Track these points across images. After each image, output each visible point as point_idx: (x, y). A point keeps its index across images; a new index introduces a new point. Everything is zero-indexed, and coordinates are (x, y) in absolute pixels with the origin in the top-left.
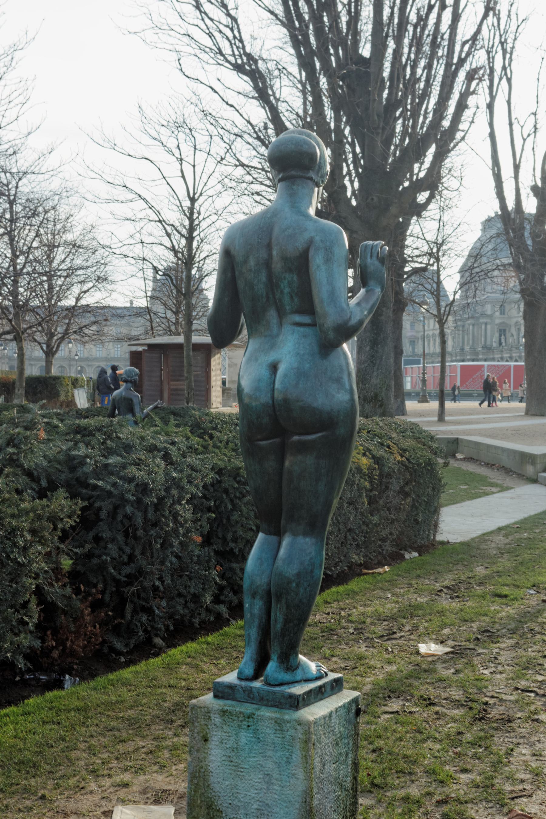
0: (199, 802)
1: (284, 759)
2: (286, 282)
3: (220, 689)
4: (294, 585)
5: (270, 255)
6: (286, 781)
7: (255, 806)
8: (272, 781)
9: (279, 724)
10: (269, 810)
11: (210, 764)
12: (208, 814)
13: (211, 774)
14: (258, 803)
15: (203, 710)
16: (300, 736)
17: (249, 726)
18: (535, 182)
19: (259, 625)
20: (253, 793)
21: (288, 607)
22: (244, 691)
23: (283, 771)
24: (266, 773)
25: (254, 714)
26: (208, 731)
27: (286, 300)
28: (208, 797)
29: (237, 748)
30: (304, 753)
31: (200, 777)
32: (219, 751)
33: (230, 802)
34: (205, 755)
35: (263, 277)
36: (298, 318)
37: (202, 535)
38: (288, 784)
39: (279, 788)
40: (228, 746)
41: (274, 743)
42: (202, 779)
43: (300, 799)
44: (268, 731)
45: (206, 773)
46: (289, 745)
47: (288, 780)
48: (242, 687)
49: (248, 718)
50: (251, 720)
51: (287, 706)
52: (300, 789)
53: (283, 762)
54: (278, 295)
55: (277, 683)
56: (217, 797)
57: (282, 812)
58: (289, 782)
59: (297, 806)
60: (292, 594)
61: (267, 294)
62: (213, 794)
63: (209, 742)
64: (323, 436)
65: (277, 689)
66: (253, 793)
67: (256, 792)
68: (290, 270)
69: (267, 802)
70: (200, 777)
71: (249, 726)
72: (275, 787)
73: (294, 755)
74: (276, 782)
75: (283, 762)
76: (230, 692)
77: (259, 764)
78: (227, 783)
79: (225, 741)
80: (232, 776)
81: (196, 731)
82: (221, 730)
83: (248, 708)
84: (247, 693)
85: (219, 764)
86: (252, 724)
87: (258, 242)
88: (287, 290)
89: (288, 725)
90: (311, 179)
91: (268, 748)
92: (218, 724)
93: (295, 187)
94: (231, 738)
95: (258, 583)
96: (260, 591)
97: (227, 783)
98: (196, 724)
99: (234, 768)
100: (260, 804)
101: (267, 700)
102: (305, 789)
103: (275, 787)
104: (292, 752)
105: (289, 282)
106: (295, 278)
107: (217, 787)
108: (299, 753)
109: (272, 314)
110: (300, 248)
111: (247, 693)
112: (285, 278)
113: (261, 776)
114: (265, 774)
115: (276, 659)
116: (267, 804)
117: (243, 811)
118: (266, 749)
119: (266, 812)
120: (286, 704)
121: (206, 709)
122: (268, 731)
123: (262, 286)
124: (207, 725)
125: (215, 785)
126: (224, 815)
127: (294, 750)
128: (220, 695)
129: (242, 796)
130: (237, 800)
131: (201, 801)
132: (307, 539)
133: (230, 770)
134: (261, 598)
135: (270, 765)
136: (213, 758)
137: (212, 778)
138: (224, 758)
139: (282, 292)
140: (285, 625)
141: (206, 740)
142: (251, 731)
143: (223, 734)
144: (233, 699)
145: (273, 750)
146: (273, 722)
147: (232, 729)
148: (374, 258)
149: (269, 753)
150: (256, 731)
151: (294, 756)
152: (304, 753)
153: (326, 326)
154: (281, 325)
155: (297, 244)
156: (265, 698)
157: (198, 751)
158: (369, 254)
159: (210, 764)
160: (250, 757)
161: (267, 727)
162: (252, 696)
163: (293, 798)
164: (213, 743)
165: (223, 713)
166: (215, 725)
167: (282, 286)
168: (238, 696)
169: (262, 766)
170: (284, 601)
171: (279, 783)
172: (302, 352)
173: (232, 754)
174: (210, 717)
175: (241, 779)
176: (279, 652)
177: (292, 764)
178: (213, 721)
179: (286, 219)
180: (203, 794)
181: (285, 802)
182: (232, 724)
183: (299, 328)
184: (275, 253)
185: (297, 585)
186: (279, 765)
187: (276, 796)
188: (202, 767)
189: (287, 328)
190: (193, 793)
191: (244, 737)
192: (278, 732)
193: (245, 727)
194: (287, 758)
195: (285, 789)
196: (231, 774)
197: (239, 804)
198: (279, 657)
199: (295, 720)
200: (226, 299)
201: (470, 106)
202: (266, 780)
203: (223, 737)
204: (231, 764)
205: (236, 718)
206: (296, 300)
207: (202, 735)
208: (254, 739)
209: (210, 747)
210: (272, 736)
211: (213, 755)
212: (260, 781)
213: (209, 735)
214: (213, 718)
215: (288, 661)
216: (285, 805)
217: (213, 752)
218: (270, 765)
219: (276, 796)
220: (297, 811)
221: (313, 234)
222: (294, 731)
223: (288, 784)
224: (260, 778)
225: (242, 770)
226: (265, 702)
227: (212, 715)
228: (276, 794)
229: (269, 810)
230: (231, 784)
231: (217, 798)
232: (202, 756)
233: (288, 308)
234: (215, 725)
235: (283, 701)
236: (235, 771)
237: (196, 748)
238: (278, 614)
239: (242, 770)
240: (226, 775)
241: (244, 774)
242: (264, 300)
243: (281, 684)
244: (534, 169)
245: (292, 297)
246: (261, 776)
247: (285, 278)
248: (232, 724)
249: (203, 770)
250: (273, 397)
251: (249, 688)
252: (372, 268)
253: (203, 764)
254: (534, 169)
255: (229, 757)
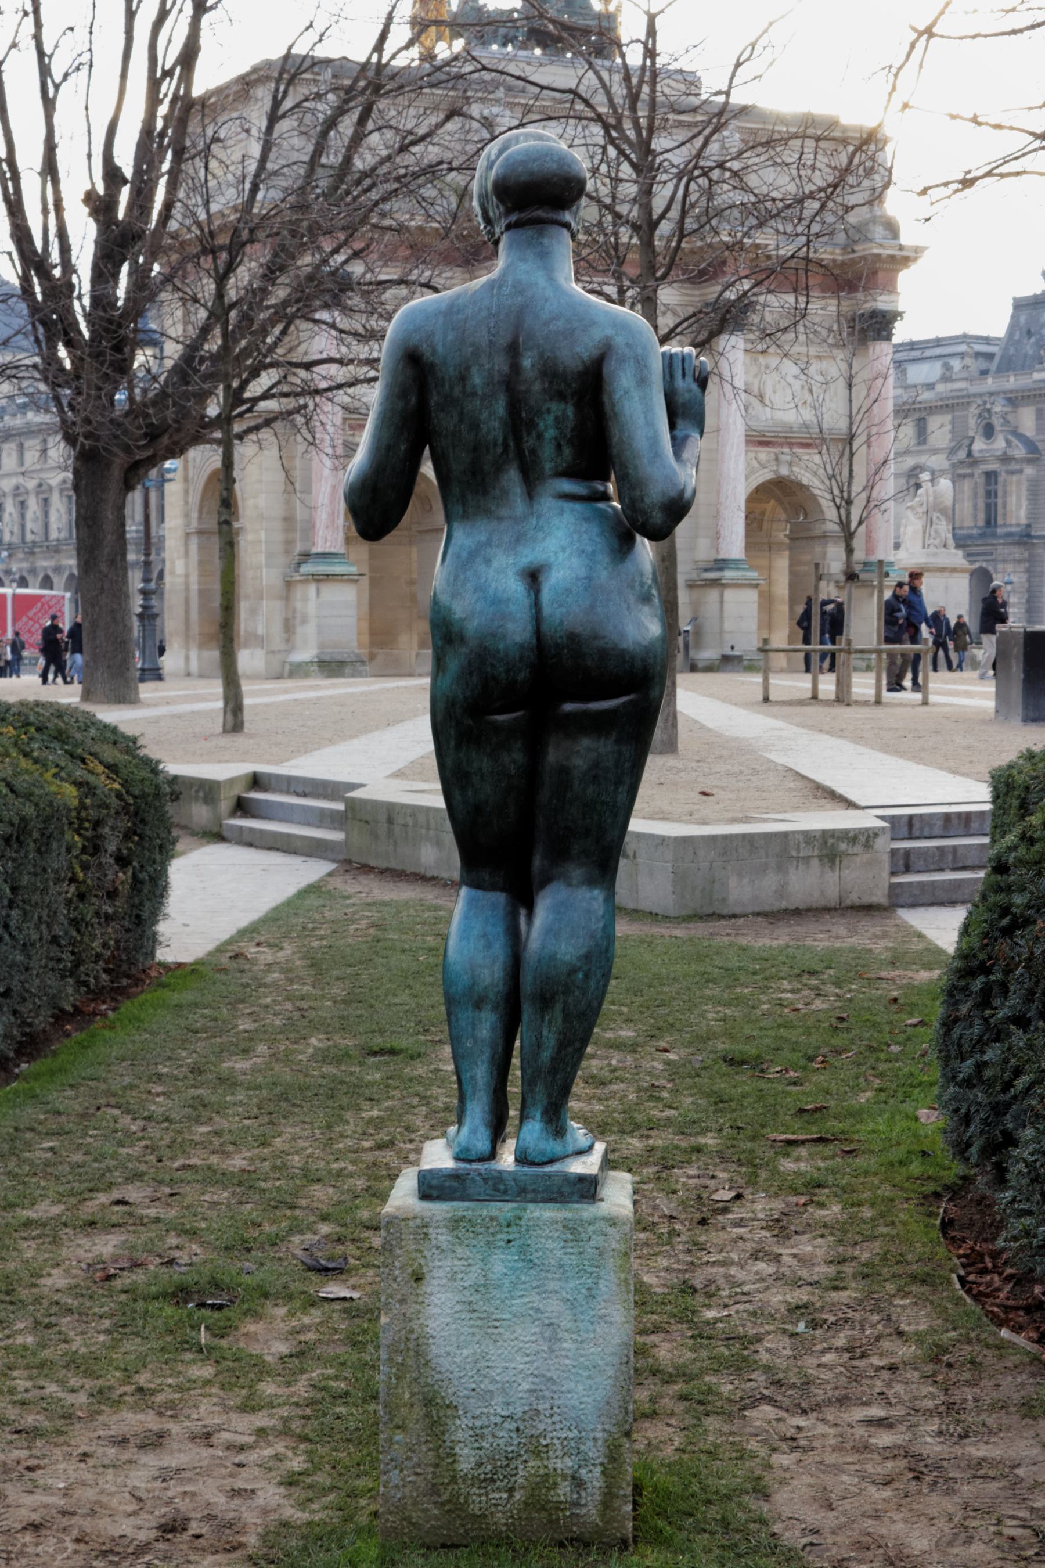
0: (407, 1396)
1: (584, 1291)
2: (550, 419)
3: (434, 1182)
4: (580, 975)
5: (515, 368)
6: (588, 1331)
7: (526, 1386)
8: (560, 1336)
9: (573, 1230)
10: (554, 1388)
11: (429, 1322)
12: (428, 1415)
13: (431, 1341)
14: (531, 1379)
15: (411, 1223)
16: (615, 1245)
17: (509, 1241)
18: (93, 184)
19: (493, 1058)
20: (520, 1362)
21: (567, 1016)
22: (485, 1180)
23: (582, 1313)
24: (547, 1321)
25: (520, 1218)
26: (422, 1262)
27: (547, 451)
28: (427, 1385)
29: (484, 1285)
30: (623, 1276)
31: (408, 1349)
32: (449, 1295)
33: (474, 1386)
34: (418, 1307)
35: (500, 407)
36: (567, 486)
37: (458, 891)
38: (592, 1335)
39: (573, 1346)
40: (466, 1284)
41: (561, 1266)
42: (411, 1353)
43: (615, 1360)
44: (550, 1245)
45: (421, 1341)
46: (592, 1265)
47: (591, 1328)
48: (480, 1174)
49: (509, 1225)
50: (513, 1229)
51: (575, 1198)
52: (617, 1340)
53: (580, 1298)
54: (529, 442)
55: (546, 1160)
56: (447, 1382)
57: (580, 1387)
58: (594, 1331)
59: (611, 1372)
60: (577, 993)
61: (505, 439)
62: (437, 1376)
63: (424, 1282)
64: (631, 701)
65: (548, 1169)
66: (520, 1362)
67: (528, 1359)
68: (561, 396)
69: (549, 1375)
70: (408, 1349)
71: (509, 1241)
72: (565, 1345)
73: (601, 1281)
74: (566, 1335)
75: (580, 1298)
76: (456, 1184)
77: (532, 1308)
78: (465, 1352)
79: (460, 1276)
80: (476, 1339)
81: (397, 1264)
82: (450, 1255)
83: (505, 1210)
84: (490, 1183)
85: (448, 1320)
86: (517, 1236)
87: (491, 341)
88: (550, 433)
89: (591, 1228)
90: (567, 226)
91: (549, 1275)
92: (444, 1246)
93: (545, 241)
94: (473, 1269)
95: (488, 981)
96: (491, 995)
97: (465, 1352)
98: (398, 1252)
99: (479, 1322)
100: (536, 1380)
101: (534, 1191)
102: (625, 1338)
103: (565, 1345)
104: (599, 1278)
105: (556, 418)
106: (570, 411)
107: (445, 1363)
108: (612, 1277)
109: (512, 477)
110: (585, 356)
111: (490, 1183)
112: (549, 411)
113: (537, 1330)
114: (544, 1325)
115: (538, 1116)
116: (551, 1379)
117: (500, 1399)
118: (546, 1278)
119: (547, 1394)
120: (573, 1193)
121: (418, 1221)
122: (550, 1245)
123: (496, 424)
124: (420, 1251)
125: (441, 1360)
126: (461, 1412)
127: (602, 1273)
128: (435, 1193)
129: (499, 1371)
130: (486, 1381)
131: (413, 1395)
132: (596, 892)
133: (471, 1326)
134: (495, 1008)
135: (553, 1306)
136: (435, 1310)
137: (433, 1347)
138: (458, 1307)
139: (540, 436)
140: (559, 1052)
141: (419, 1279)
142: (514, 1250)
143: (456, 1262)
144: (462, 1199)
145: (560, 1279)
146: (560, 1227)
147: (474, 1251)
148: (689, 379)
149: (552, 1285)
150: (524, 1249)
151: (602, 1283)
152: (623, 1276)
153: (647, 500)
154: (530, 494)
155: (578, 349)
156: (530, 1188)
157: (403, 1301)
158: (680, 372)
159: (429, 1322)
160: (513, 1298)
161: (547, 1238)
162: (502, 1187)
163: (602, 1359)
164: (435, 1282)
165: (455, 1223)
166: (438, 1248)
167: (542, 425)
168: (471, 1191)
169: (538, 1310)
170: (559, 1007)
171: (574, 1336)
172: (589, 549)
173: (475, 1298)
174: (426, 1234)
175: (495, 1341)
176: (545, 1102)
177: (599, 1299)
178: (434, 1242)
179: (546, 300)
180: (416, 1380)
181: (587, 1368)
182: (474, 1242)
183: (571, 505)
184: (527, 363)
185: (587, 976)
186: (571, 1303)
187: (567, 1362)
188: (412, 1331)
189: (547, 504)
190: (394, 1381)
191: (500, 1263)
192: (570, 1244)
193: (502, 1244)
194: (588, 1289)
195: (585, 1345)
196: (473, 1334)
197: (492, 1387)
198: (545, 1113)
199: (604, 1219)
200: (403, 448)
201: (870, 123)
202: (547, 1335)
203: (455, 1269)
204: (475, 1315)
205: (482, 1230)
206: (567, 451)
207: (410, 1270)
208: (521, 1264)
209: (429, 1290)
210: (559, 1254)
211: (436, 1305)
212: (534, 1338)
213: (425, 1270)
214: (433, 1236)
215: (558, 1119)
216: (586, 1374)
217: (434, 1299)
218: (553, 1306)
219: (567, 1362)
220: (611, 1382)
221: (609, 332)
222: (601, 1238)
223: (592, 1335)
224: (535, 1334)
225: (497, 1324)
226: (529, 1196)
227: (431, 1230)
228: (567, 1357)
229: (554, 1388)
230: (474, 1354)
231: (445, 1383)
232: (411, 1309)
233: (548, 466)
234: (438, 1248)
235: (566, 1189)
236: (481, 1327)
237: (399, 1297)
238: (545, 1032)
239: (497, 1324)
240: (463, 1338)
241: (501, 1330)
242: (499, 450)
243: (551, 1162)
244: (89, 156)
245: (559, 447)
246: (537, 1330)
247: (549, 411)
248: (474, 1242)
249: (414, 1336)
250: (538, 632)
251: (496, 1174)
252: (687, 396)
253: (414, 1325)
254: (89, 156)
255: (470, 1303)
